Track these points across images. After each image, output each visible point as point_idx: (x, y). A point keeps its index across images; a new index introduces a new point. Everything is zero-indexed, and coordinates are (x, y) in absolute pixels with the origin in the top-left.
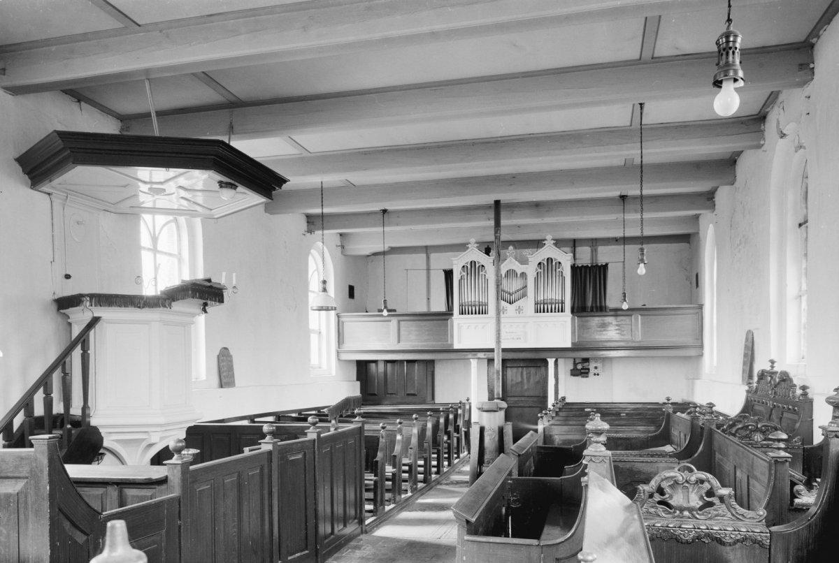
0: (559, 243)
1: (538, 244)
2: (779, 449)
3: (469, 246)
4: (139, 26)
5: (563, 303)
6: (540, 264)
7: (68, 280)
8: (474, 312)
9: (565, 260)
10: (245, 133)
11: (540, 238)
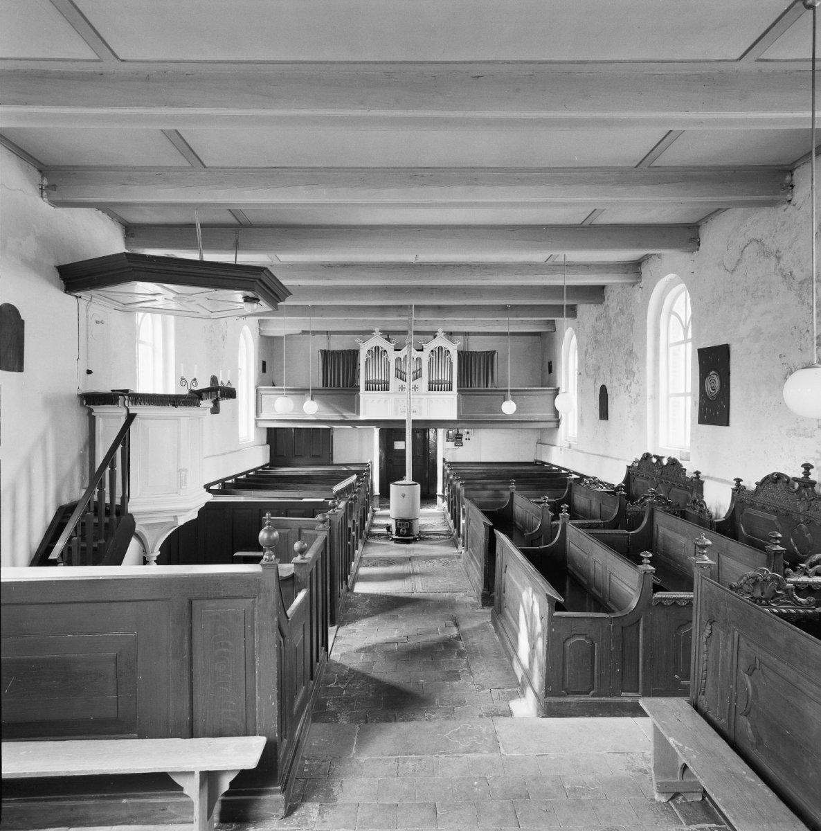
0: (450, 334)
1: (434, 334)
2: (777, 544)
3: (374, 334)
4: (205, 167)
5: (451, 383)
6: (432, 351)
7: (90, 375)
8: (377, 389)
9: (453, 349)
10: (250, 250)
11: (434, 330)
